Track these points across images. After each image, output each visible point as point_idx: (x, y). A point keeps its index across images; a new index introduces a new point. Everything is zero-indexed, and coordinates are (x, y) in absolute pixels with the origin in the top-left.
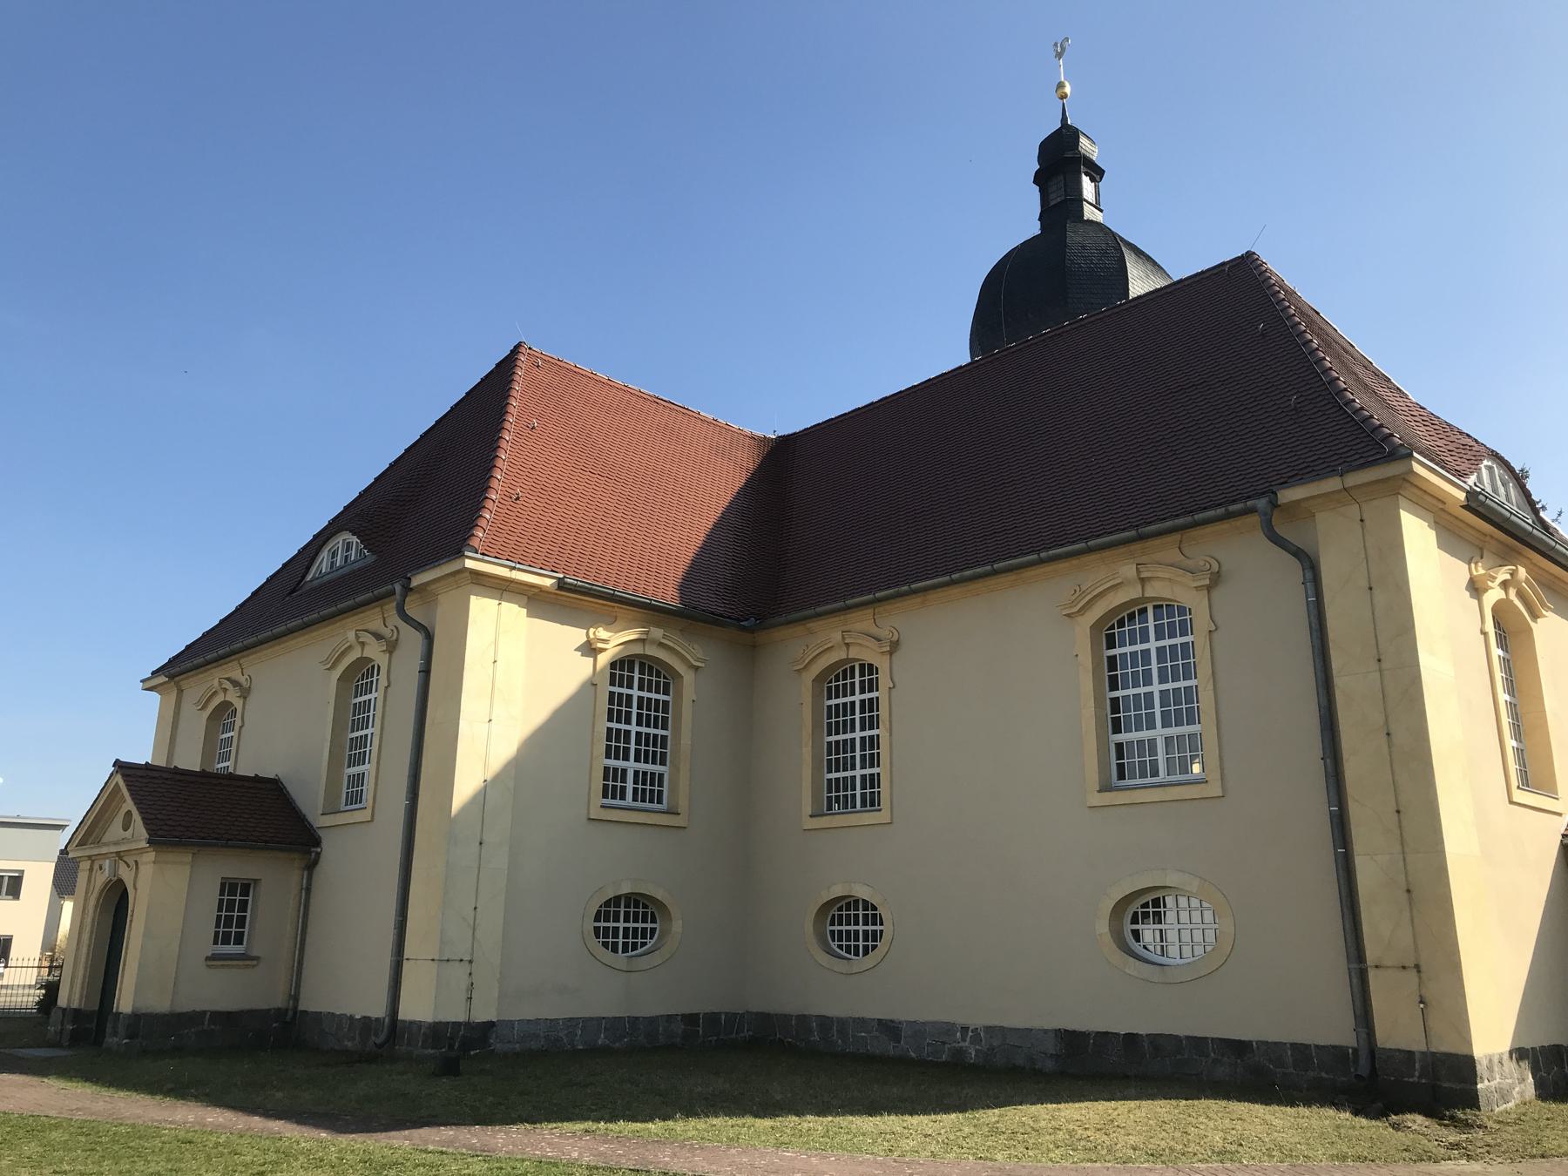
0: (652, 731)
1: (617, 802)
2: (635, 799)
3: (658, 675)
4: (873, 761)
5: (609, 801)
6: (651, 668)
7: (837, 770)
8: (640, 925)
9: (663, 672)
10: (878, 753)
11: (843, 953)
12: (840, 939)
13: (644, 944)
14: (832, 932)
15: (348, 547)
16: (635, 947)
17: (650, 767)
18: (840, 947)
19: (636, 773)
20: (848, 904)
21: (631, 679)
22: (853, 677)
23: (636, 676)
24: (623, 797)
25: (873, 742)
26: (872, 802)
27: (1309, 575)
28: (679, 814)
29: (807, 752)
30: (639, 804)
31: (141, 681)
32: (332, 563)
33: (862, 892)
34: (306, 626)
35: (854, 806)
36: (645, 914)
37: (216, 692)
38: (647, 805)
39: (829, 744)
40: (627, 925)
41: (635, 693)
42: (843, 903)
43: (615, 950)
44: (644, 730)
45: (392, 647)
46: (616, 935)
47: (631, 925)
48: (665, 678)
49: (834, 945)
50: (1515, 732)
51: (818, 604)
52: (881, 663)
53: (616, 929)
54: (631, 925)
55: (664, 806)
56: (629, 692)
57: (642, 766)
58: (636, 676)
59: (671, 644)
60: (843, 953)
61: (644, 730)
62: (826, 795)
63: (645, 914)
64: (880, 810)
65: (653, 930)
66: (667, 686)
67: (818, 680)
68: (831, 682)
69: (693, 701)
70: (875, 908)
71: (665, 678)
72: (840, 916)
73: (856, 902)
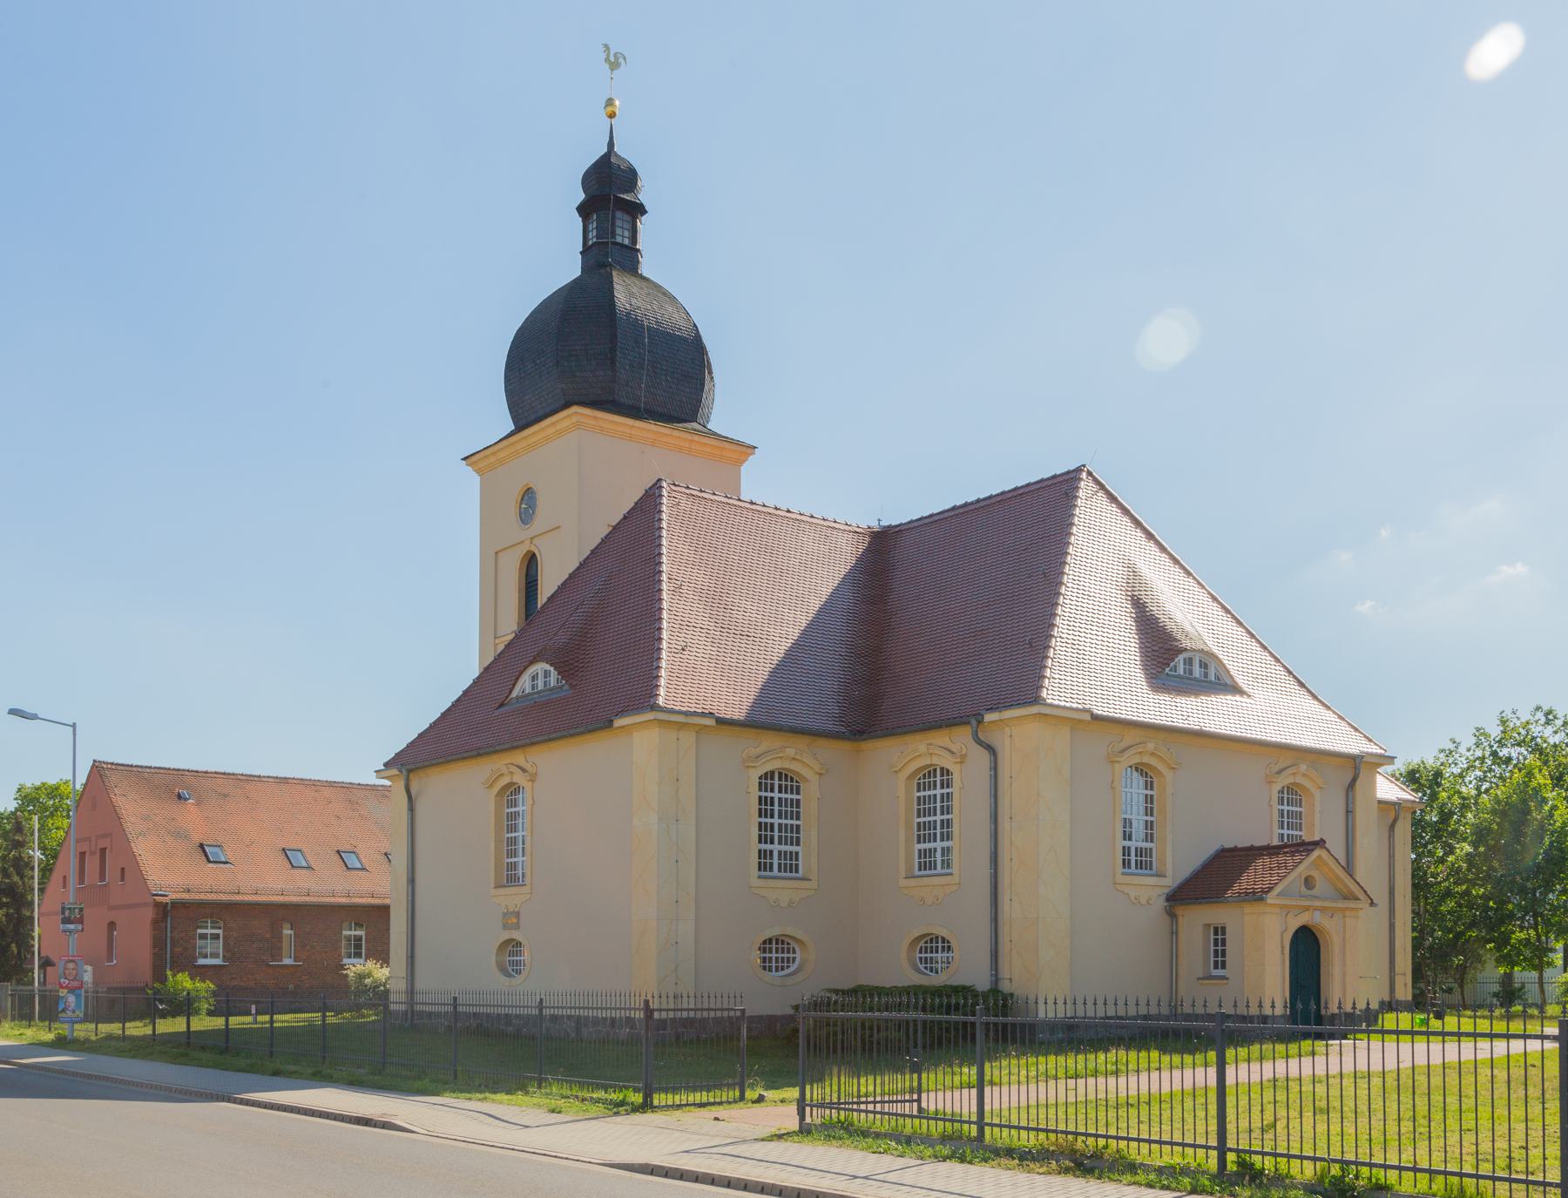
1: (768, 873)
2: (780, 871)
5: (763, 873)
6: (786, 775)
8: (786, 955)
11: (928, 972)
12: (926, 963)
13: (788, 967)
14: (921, 958)
15: (547, 674)
16: (783, 969)
17: (789, 848)
18: (926, 968)
19: (780, 852)
20: (931, 940)
23: (776, 782)
24: (771, 870)
27: (991, 751)
28: (810, 880)
30: (783, 874)
31: (376, 772)
32: (533, 685)
33: (942, 932)
34: (572, 735)
36: (788, 949)
37: (502, 775)
38: (788, 874)
40: (777, 955)
41: (776, 795)
42: (928, 938)
43: (770, 970)
44: (783, 821)
45: (962, 759)
46: (770, 962)
47: (780, 955)
49: (922, 967)
51: (658, 421)
53: (770, 958)
54: (780, 955)
55: (800, 874)
57: (784, 848)
58: (776, 782)
59: (1161, 755)
60: (928, 972)
61: (783, 821)
63: (788, 949)
65: (794, 959)
66: (798, 788)
67: (910, 777)
69: (818, 799)
70: (948, 942)
72: (926, 948)
73: (937, 937)
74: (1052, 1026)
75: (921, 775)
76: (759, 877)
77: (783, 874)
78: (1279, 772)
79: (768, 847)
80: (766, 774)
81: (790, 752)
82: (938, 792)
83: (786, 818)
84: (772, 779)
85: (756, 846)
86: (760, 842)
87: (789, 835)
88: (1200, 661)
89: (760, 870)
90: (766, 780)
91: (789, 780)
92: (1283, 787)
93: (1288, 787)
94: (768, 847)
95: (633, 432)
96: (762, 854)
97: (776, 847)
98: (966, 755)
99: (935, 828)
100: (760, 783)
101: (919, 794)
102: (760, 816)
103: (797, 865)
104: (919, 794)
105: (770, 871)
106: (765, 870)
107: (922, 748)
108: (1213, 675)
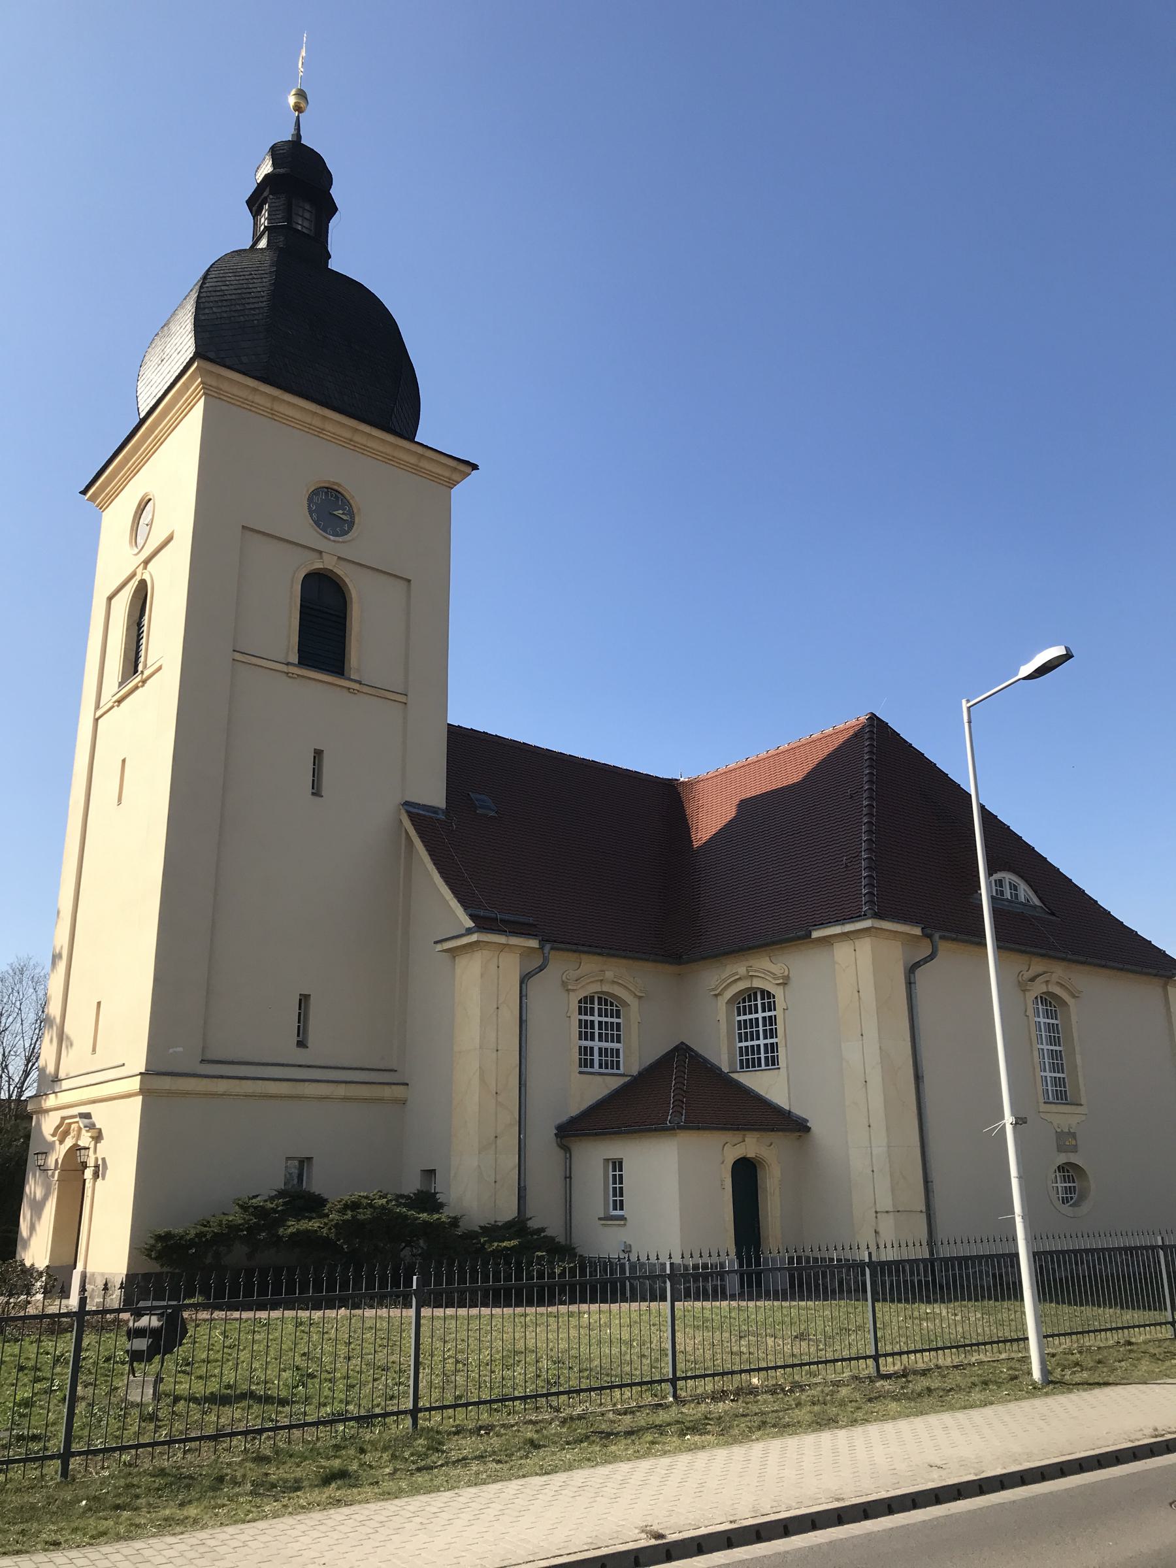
0: (609, 1020)
2: (600, 1067)
3: (612, 1005)
4: (772, 1034)
5: (583, 1069)
6: (606, 1000)
7: (746, 1040)
9: (615, 1003)
10: (776, 1028)
17: (609, 1045)
19: (600, 1049)
21: (592, 1009)
22: (756, 1000)
23: (596, 1007)
25: (772, 1020)
26: (773, 1062)
29: (723, 1026)
30: (603, 1070)
35: (760, 1065)
38: (609, 1071)
39: (739, 1022)
41: (596, 1019)
44: (604, 1019)
48: (616, 1006)
50: (1156, 1277)
52: (778, 992)
55: (621, 1071)
56: (592, 1018)
57: (604, 1045)
58: (596, 1007)
61: (604, 1019)
62: (737, 1032)
64: (779, 1068)
67: (730, 1001)
68: (739, 1003)
71: (616, 1006)
74: (880, 1268)
75: (740, 999)
76: (580, 1073)
77: (603, 1070)
78: (1032, 980)
79: (589, 1043)
80: (586, 998)
81: (609, 975)
82: (760, 1015)
83: (606, 1016)
84: (592, 1002)
85: (577, 1043)
86: (580, 1039)
87: (609, 1059)
88: (1010, 883)
89: (580, 1066)
90: (585, 1008)
91: (608, 1004)
92: (1036, 998)
93: (1041, 997)
94: (589, 1043)
95: (276, 407)
96: (584, 1051)
97: (596, 1044)
98: (788, 976)
99: (759, 1053)
100: (580, 1008)
101: (739, 1018)
102: (580, 1014)
103: (618, 1062)
104: (739, 1018)
105: (602, 1022)
106: (586, 1066)
107: (742, 970)
108: (1023, 897)
